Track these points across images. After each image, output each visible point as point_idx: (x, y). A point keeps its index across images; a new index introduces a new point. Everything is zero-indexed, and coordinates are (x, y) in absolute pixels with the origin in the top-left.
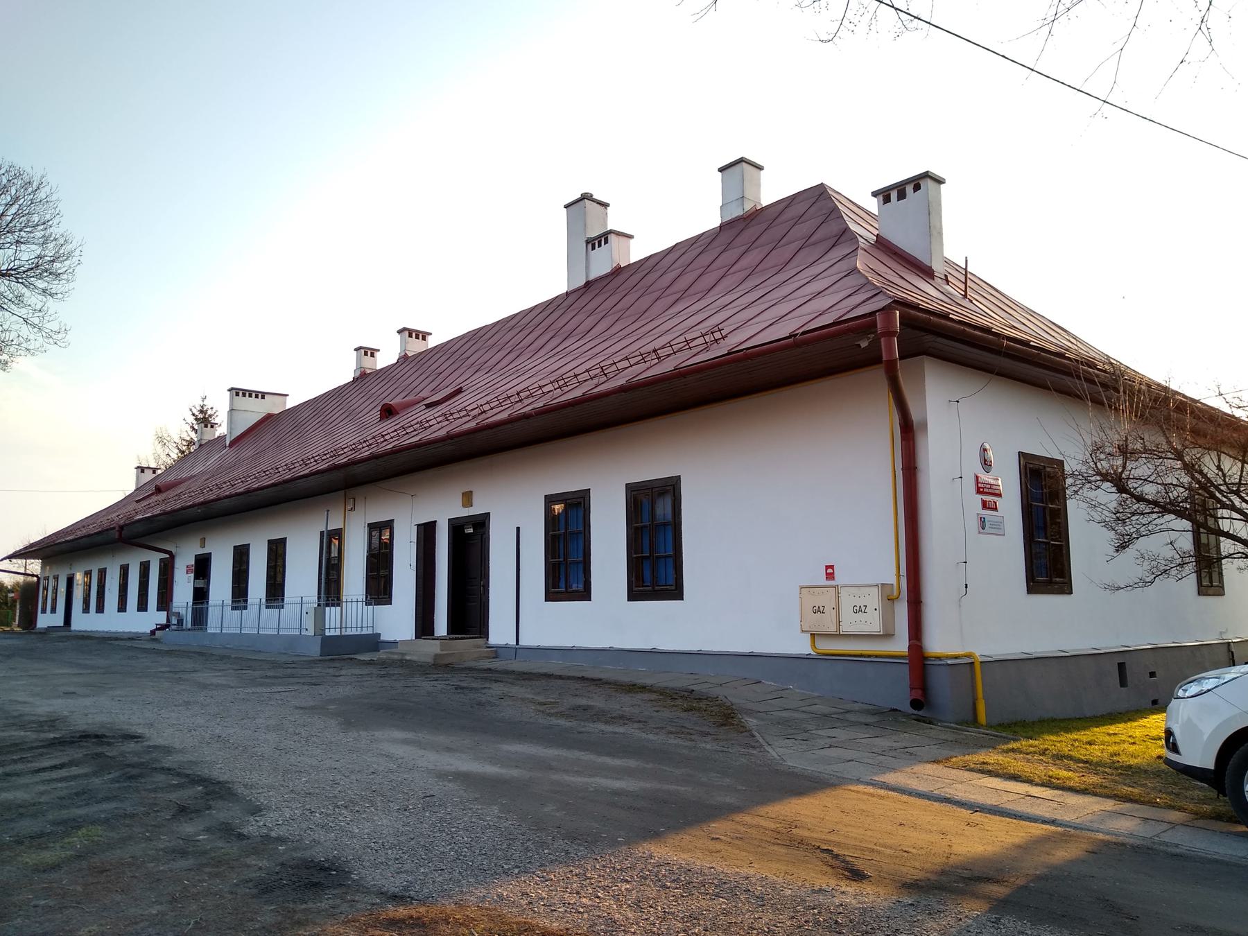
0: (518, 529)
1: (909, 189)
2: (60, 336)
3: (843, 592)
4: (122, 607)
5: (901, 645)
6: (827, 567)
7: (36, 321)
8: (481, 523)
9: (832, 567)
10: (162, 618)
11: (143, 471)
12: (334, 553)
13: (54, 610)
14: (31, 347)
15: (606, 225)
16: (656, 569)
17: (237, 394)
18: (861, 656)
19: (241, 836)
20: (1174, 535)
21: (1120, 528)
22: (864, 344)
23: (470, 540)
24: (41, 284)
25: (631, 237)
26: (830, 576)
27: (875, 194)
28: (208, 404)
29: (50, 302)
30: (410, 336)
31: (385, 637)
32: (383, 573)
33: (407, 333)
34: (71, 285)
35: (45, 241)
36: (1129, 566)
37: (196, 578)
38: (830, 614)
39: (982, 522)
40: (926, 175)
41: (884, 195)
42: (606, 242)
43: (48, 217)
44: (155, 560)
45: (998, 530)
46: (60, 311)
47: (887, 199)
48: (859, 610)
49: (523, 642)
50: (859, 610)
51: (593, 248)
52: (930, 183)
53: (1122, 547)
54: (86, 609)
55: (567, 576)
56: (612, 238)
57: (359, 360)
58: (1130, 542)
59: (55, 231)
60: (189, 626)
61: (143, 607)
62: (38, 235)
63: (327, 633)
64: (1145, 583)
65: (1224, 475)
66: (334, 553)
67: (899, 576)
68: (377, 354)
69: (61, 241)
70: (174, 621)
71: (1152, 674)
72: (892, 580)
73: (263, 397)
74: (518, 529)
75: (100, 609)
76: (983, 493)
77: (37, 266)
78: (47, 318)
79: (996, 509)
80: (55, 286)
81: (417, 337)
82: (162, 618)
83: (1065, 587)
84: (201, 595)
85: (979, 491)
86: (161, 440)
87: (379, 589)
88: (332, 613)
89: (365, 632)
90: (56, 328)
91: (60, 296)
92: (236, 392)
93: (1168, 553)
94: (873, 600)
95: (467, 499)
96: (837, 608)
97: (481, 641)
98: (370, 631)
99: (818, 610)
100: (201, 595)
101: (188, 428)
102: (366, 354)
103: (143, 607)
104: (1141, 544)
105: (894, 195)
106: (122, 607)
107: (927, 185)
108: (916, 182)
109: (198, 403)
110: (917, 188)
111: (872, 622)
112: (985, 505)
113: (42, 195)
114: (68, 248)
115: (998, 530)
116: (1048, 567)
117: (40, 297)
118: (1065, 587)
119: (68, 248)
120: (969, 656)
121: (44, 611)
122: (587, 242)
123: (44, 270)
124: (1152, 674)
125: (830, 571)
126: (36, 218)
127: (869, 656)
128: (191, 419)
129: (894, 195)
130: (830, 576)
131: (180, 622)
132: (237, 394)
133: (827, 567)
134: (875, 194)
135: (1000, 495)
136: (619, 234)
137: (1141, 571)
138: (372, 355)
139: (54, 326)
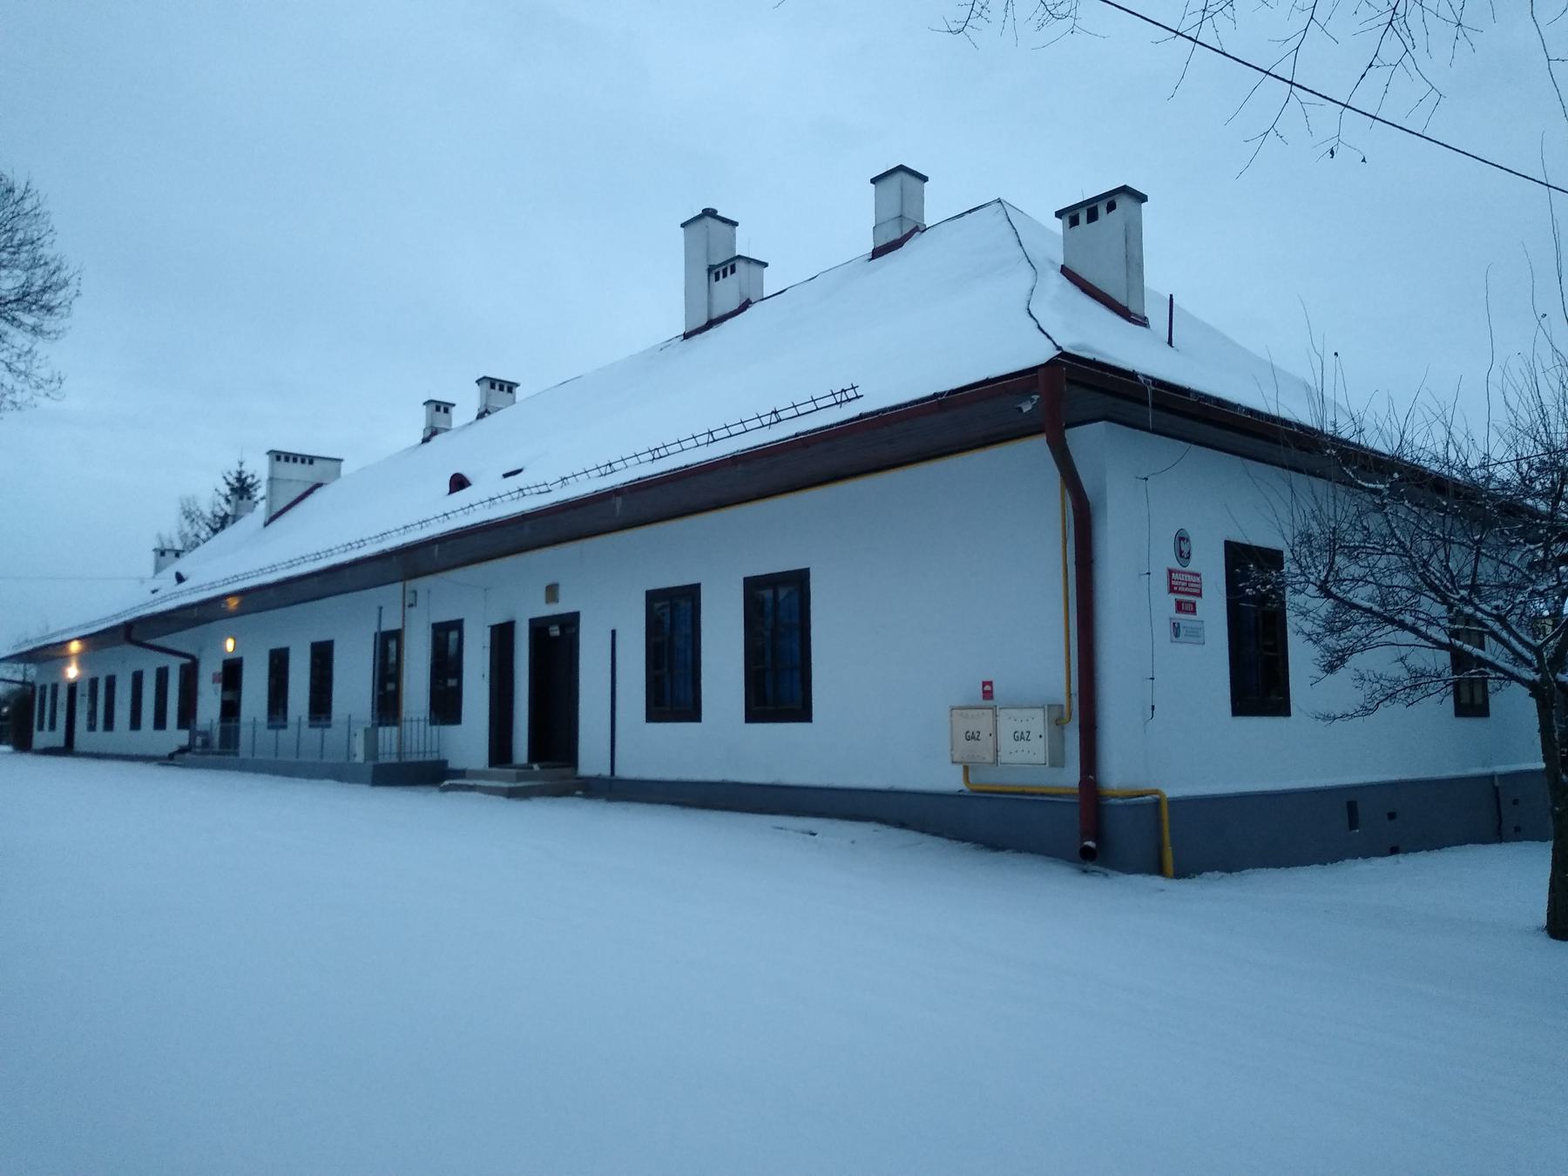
0: (614, 632)
1: (1102, 209)
2: (55, 385)
3: (1002, 714)
4: (135, 723)
5: (1070, 776)
6: (984, 684)
7: (21, 366)
8: (570, 622)
9: (990, 683)
10: (183, 737)
11: (163, 554)
12: (392, 659)
13: (53, 726)
14: (18, 400)
15: (734, 250)
16: (779, 688)
17: (278, 458)
18: (1023, 793)
19: (1460, 660)
20: (1404, 651)
21: (1330, 641)
22: (1027, 407)
23: (556, 645)
24: (29, 320)
25: (766, 265)
26: (988, 695)
27: (1059, 214)
28: (248, 469)
29: (41, 346)
30: (493, 387)
31: (451, 765)
32: (452, 683)
33: (433, 406)
34: (65, 323)
35: (35, 263)
36: (1342, 690)
37: (225, 689)
38: (986, 741)
39: (1176, 629)
40: (1125, 190)
41: (1070, 215)
42: (733, 271)
43: (36, 235)
44: (174, 665)
45: (1197, 635)
46: (51, 356)
47: (1074, 222)
48: (1019, 737)
49: (617, 773)
50: (1019, 737)
51: (717, 279)
52: (1123, 203)
53: (1331, 668)
54: (92, 727)
55: (672, 693)
56: (740, 266)
57: (430, 418)
58: (1342, 660)
59: (46, 252)
60: (217, 749)
61: (160, 723)
62: (23, 256)
63: (381, 760)
64: (1367, 711)
65: (1452, 577)
66: (392, 659)
67: (1069, 695)
68: (453, 410)
69: (52, 267)
70: (199, 741)
71: (1392, 816)
72: (1063, 700)
73: (311, 462)
74: (614, 632)
75: (109, 724)
76: (1178, 592)
77: (25, 295)
78: (36, 363)
79: (1194, 612)
80: (49, 323)
81: (501, 389)
82: (183, 737)
83: (1281, 707)
84: (230, 710)
85: (1172, 590)
86: (188, 515)
87: (446, 706)
88: (387, 734)
89: (428, 758)
90: (47, 376)
91: (53, 335)
92: (278, 456)
93: (1398, 671)
94: (1037, 723)
95: (552, 592)
96: (995, 734)
97: (567, 771)
98: (435, 757)
99: (972, 737)
100: (230, 710)
101: (222, 501)
102: (438, 409)
103: (160, 723)
104: (1355, 661)
105: (1083, 217)
106: (135, 723)
107: (1123, 203)
108: (1110, 200)
109: (235, 468)
110: (1111, 207)
111: (1036, 750)
112: (1180, 607)
113: (27, 205)
114: (63, 275)
115: (1197, 635)
116: (1259, 685)
117: (30, 336)
118: (1281, 707)
119: (63, 275)
120: (1156, 792)
121: (41, 728)
122: (710, 269)
123: (33, 302)
124: (1392, 816)
125: (987, 688)
126: (20, 235)
127: (1033, 794)
128: (226, 490)
129: (1083, 217)
130: (988, 695)
131: (206, 743)
132: (278, 458)
133: (984, 684)
134: (1059, 214)
135: (1200, 595)
136: (749, 260)
137: (1358, 697)
138: (446, 411)
139: (45, 373)
